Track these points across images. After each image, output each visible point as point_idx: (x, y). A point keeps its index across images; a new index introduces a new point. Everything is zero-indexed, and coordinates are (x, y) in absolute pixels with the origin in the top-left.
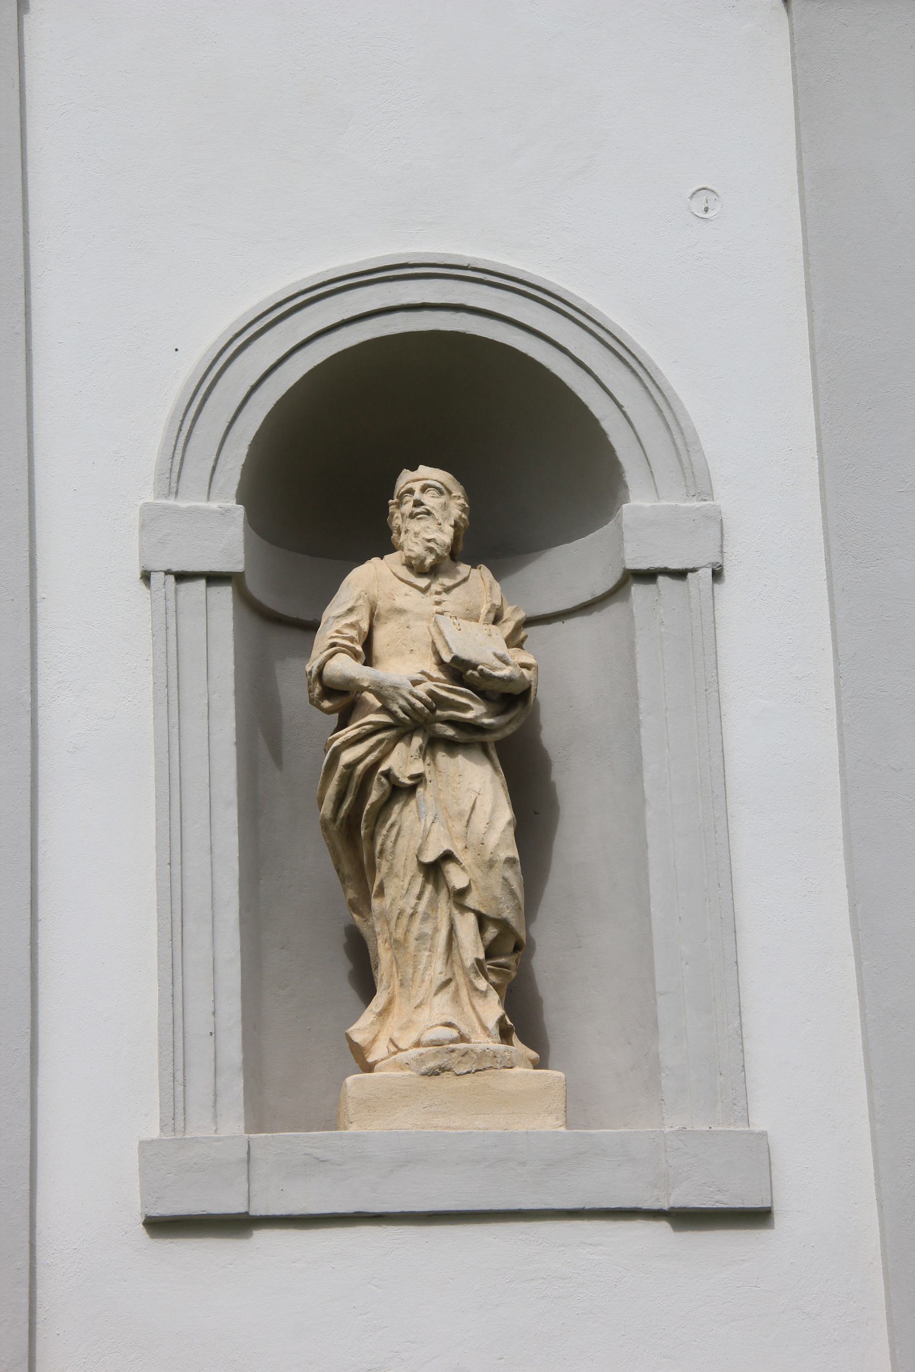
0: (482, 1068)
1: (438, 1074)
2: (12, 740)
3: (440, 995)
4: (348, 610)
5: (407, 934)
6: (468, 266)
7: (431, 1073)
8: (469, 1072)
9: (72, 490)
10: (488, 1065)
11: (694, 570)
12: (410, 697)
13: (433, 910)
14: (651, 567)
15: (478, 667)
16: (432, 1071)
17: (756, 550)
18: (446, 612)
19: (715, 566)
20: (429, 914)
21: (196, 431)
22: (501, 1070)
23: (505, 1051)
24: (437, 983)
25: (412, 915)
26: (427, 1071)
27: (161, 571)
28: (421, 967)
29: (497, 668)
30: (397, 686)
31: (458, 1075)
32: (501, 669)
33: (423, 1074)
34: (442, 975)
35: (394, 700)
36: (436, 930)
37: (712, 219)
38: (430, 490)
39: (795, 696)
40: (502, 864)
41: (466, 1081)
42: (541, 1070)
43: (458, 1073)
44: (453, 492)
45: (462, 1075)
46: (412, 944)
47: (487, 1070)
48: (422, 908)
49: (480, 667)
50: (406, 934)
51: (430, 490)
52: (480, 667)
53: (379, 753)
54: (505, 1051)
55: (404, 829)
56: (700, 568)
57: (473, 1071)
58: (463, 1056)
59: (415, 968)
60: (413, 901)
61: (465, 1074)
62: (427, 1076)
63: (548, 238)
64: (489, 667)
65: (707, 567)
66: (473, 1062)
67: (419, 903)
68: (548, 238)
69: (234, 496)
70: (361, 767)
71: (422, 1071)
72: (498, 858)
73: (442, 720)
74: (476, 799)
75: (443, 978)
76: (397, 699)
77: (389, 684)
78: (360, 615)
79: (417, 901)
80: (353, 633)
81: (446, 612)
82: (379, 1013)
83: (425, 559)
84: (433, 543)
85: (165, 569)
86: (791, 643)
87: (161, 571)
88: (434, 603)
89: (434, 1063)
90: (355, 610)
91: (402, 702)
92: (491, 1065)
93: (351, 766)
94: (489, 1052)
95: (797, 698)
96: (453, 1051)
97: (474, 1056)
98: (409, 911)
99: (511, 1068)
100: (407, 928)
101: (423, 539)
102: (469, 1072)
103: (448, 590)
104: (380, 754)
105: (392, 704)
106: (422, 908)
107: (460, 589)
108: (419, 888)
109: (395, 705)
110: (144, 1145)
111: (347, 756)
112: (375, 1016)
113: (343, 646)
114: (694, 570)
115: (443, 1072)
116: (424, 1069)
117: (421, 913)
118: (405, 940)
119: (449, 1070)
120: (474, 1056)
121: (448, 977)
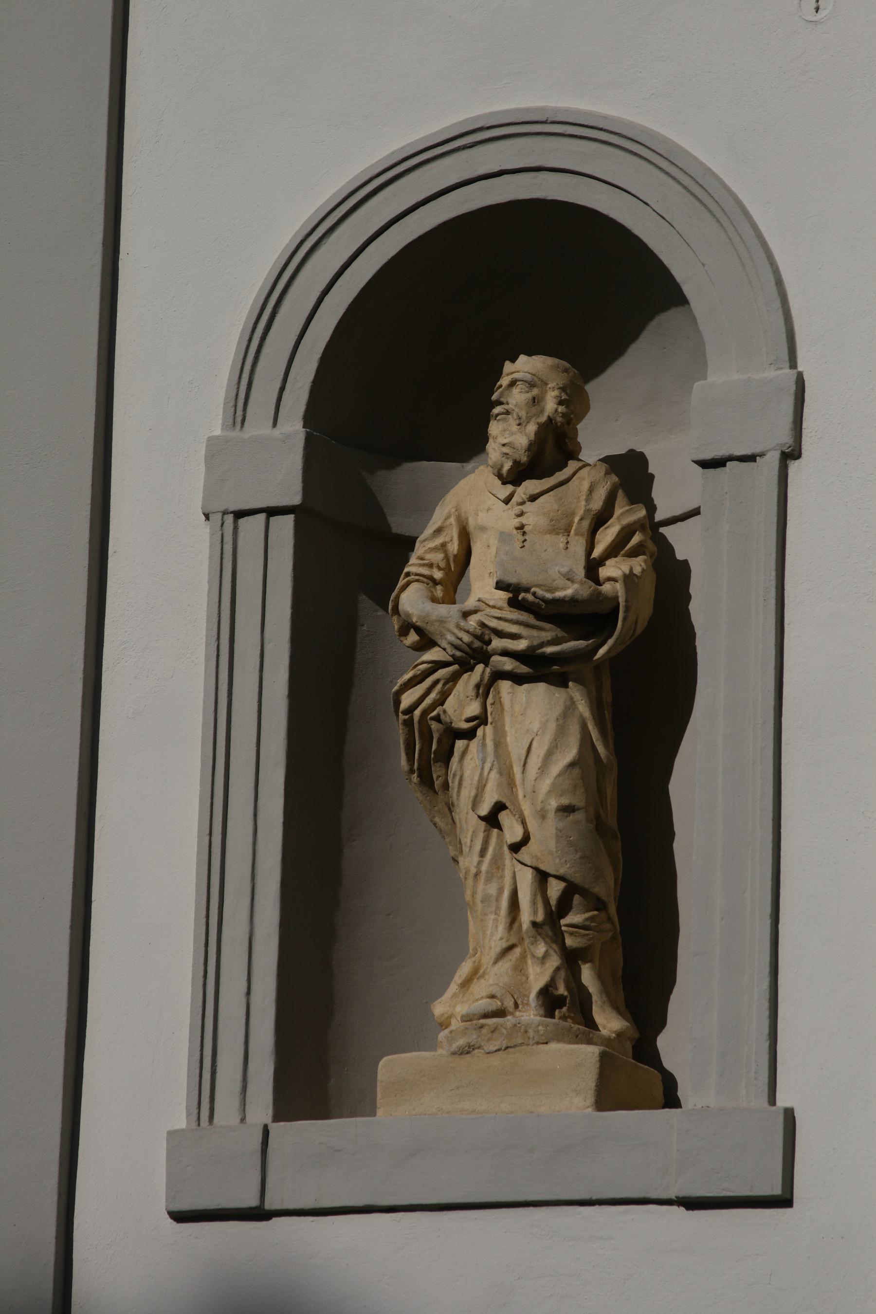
0: (512, 1045)
1: (468, 1053)
2: (65, 711)
3: (500, 963)
4: (434, 532)
5: (475, 896)
6: (547, 120)
7: (460, 1051)
8: (499, 1050)
9: (148, 429)
10: (520, 1041)
11: (762, 455)
12: (456, 631)
13: (498, 868)
14: (716, 456)
15: (531, 589)
16: (461, 1049)
17: (839, 422)
18: (527, 525)
19: (783, 447)
20: (493, 873)
21: (265, 350)
22: (534, 1047)
23: (539, 1025)
24: (497, 950)
25: (476, 875)
26: (456, 1049)
27: (218, 512)
28: (488, 932)
29: (557, 588)
30: (443, 619)
31: (488, 1053)
32: (564, 589)
33: (454, 1053)
34: (503, 940)
35: (443, 636)
36: (501, 890)
37: (822, 21)
38: (518, 385)
39: (868, 595)
40: (553, 814)
41: (495, 1061)
42: (408, 1055)
43: (487, 1051)
44: (549, 382)
45: (492, 1053)
46: (479, 906)
47: (519, 1046)
48: (484, 868)
49: (533, 590)
50: (473, 896)
51: (518, 385)
52: (533, 590)
53: (437, 694)
54: (539, 1025)
55: (466, 779)
56: (768, 451)
57: (503, 1048)
58: (492, 1032)
59: (484, 933)
60: (476, 858)
61: (496, 1051)
62: (457, 1055)
63: (640, 72)
64: (546, 588)
65: (775, 450)
66: (503, 1038)
67: (483, 861)
68: (640, 72)
69: (301, 418)
70: (417, 713)
71: (451, 1050)
72: (549, 807)
73: (499, 652)
74: (533, 740)
75: (504, 944)
76: (445, 635)
77: (435, 618)
78: (449, 536)
79: (481, 859)
80: (437, 558)
81: (527, 525)
82: (461, 984)
83: (502, 466)
84: (508, 447)
85: (222, 509)
86: (868, 532)
87: (218, 512)
88: (514, 516)
89: (463, 1040)
90: (444, 531)
91: (450, 637)
92: (522, 1041)
93: (410, 710)
94: (520, 1027)
95: (870, 598)
96: (482, 1027)
97: (504, 1032)
98: (473, 870)
99: (547, 1043)
100: (474, 889)
101: (499, 444)
102: (499, 1050)
103: (533, 498)
104: (438, 696)
105: (440, 640)
106: (484, 868)
107: (549, 496)
108: (481, 844)
109: (444, 641)
110: (171, 1134)
111: (407, 700)
112: (457, 987)
113: (416, 575)
114: (762, 455)
115: (473, 1049)
116: (454, 1047)
117: (484, 872)
118: (474, 903)
119: (479, 1048)
120: (504, 1032)
121: (510, 943)
